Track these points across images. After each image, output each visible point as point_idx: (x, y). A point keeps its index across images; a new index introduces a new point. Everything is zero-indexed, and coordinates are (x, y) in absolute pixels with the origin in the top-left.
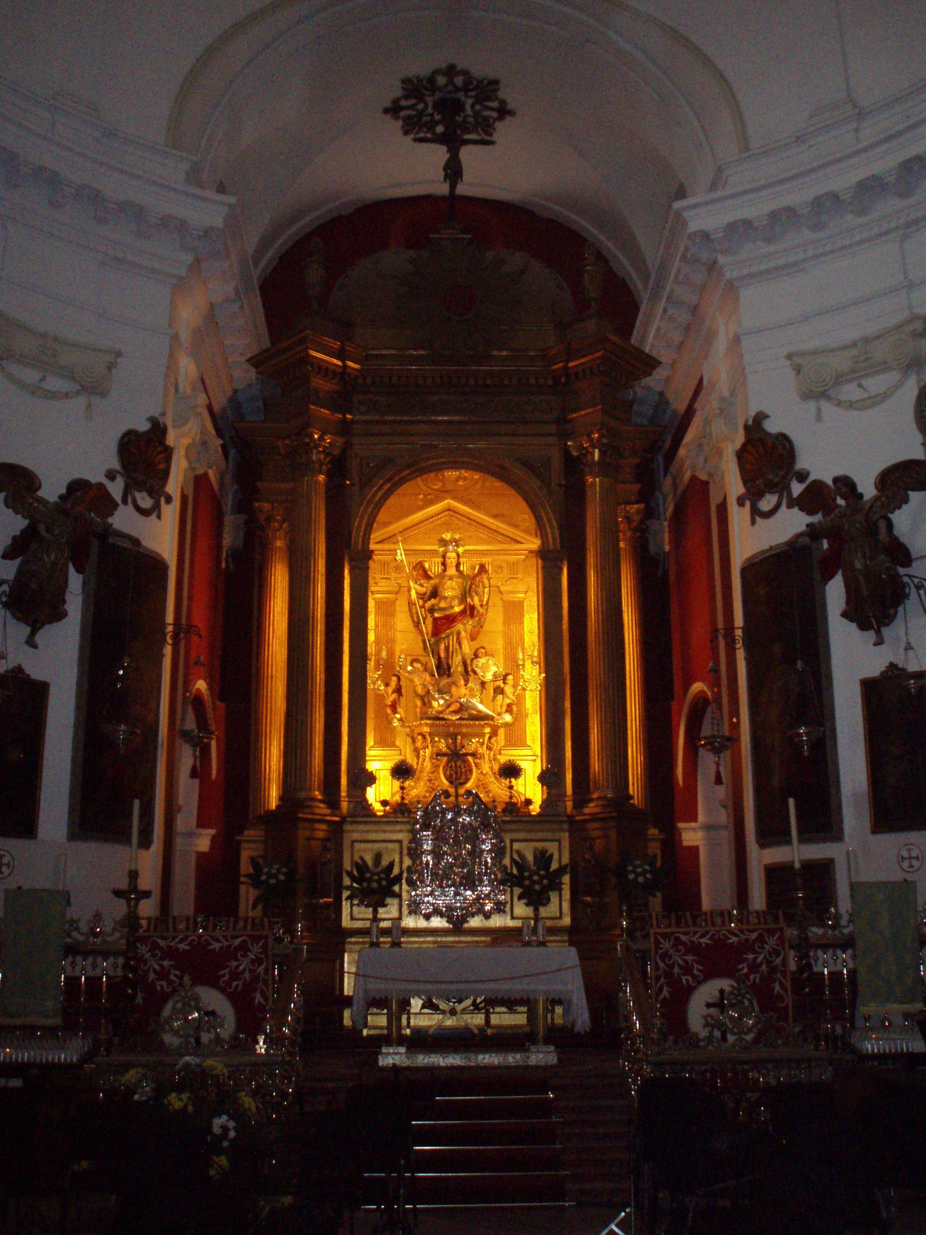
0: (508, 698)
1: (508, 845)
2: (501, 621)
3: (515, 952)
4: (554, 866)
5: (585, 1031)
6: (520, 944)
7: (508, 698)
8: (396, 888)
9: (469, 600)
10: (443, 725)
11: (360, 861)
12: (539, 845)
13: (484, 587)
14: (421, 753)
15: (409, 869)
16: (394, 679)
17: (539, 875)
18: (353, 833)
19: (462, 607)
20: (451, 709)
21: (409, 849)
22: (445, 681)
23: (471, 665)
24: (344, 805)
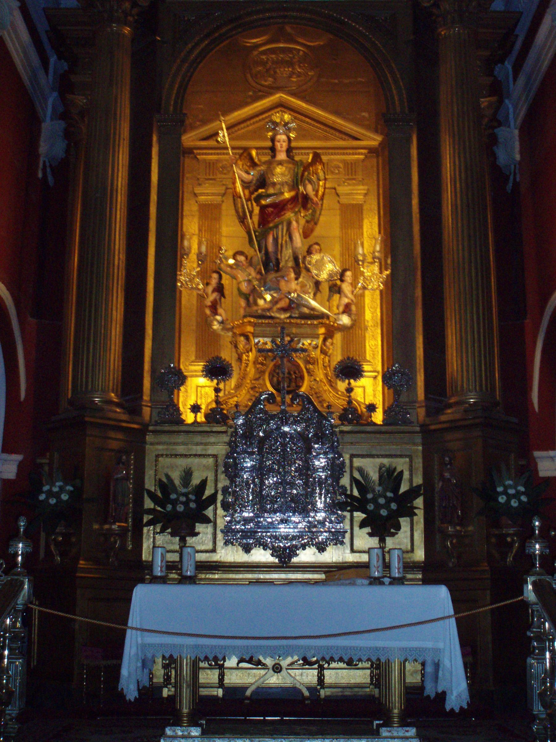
0: (347, 297)
1: (347, 462)
2: (338, 225)
3: (361, 594)
4: (404, 488)
5: (461, 708)
6: (366, 582)
7: (347, 297)
8: (209, 512)
9: (301, 188)
10: (268, 325)
11: (164, 480)
12: (386, 461)
13: (319, 180)
14: (244, 357)
15: (225, 490)
16: (215, 276)
17: (385, 497)
18: (154, 446)
19: (293, 193)
20: (279, 306)
21: (226, 465)
22: (272, 276)
23: (304, 263)
24: (146, 411)
